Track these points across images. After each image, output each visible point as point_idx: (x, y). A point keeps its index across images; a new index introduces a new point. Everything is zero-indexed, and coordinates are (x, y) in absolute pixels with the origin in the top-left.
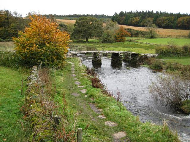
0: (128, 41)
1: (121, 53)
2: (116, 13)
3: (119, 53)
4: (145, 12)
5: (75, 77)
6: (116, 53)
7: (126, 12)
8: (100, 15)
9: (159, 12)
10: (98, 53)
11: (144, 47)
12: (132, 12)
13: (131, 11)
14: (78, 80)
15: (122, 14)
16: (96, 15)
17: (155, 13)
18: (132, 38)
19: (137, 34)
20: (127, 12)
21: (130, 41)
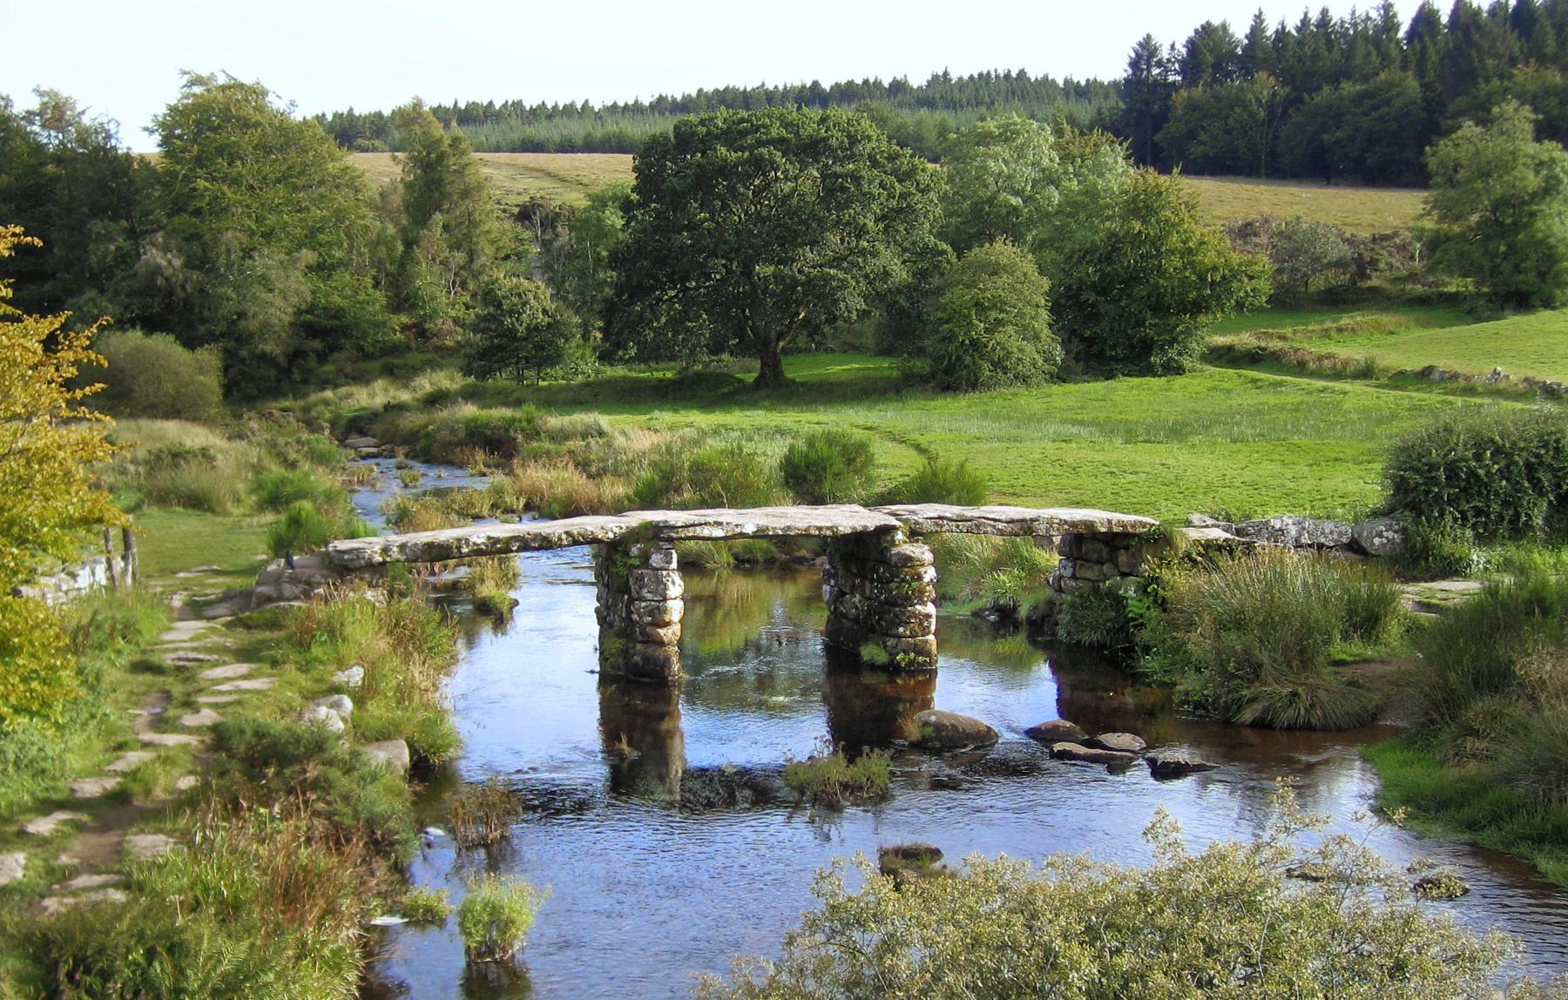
9: (1240, 31)
12: (1335, 16)
13: (1324, 12)
15: (1208, 47)
16: (940, 81)
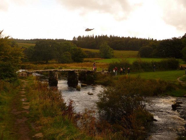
0: (85, 61)
1: (76, 71)
2: (74, 37)
3: (74, 71)
4: (154, 40)
5: (23, 94)
6: (72, 71)
7: (83, 36)
8: (50, 39)
10: (54, 71)
11: (100, 66)
13: (88, 36)
14: (25, 97)
17: (109, 37)
18: (90, 59)
19: (93, 56)
20: (84, 37)
21: (88, 61)
